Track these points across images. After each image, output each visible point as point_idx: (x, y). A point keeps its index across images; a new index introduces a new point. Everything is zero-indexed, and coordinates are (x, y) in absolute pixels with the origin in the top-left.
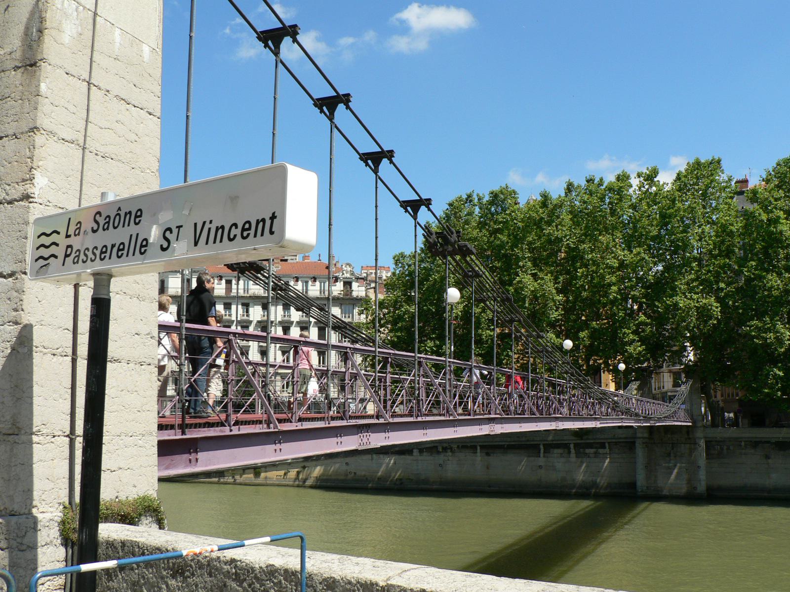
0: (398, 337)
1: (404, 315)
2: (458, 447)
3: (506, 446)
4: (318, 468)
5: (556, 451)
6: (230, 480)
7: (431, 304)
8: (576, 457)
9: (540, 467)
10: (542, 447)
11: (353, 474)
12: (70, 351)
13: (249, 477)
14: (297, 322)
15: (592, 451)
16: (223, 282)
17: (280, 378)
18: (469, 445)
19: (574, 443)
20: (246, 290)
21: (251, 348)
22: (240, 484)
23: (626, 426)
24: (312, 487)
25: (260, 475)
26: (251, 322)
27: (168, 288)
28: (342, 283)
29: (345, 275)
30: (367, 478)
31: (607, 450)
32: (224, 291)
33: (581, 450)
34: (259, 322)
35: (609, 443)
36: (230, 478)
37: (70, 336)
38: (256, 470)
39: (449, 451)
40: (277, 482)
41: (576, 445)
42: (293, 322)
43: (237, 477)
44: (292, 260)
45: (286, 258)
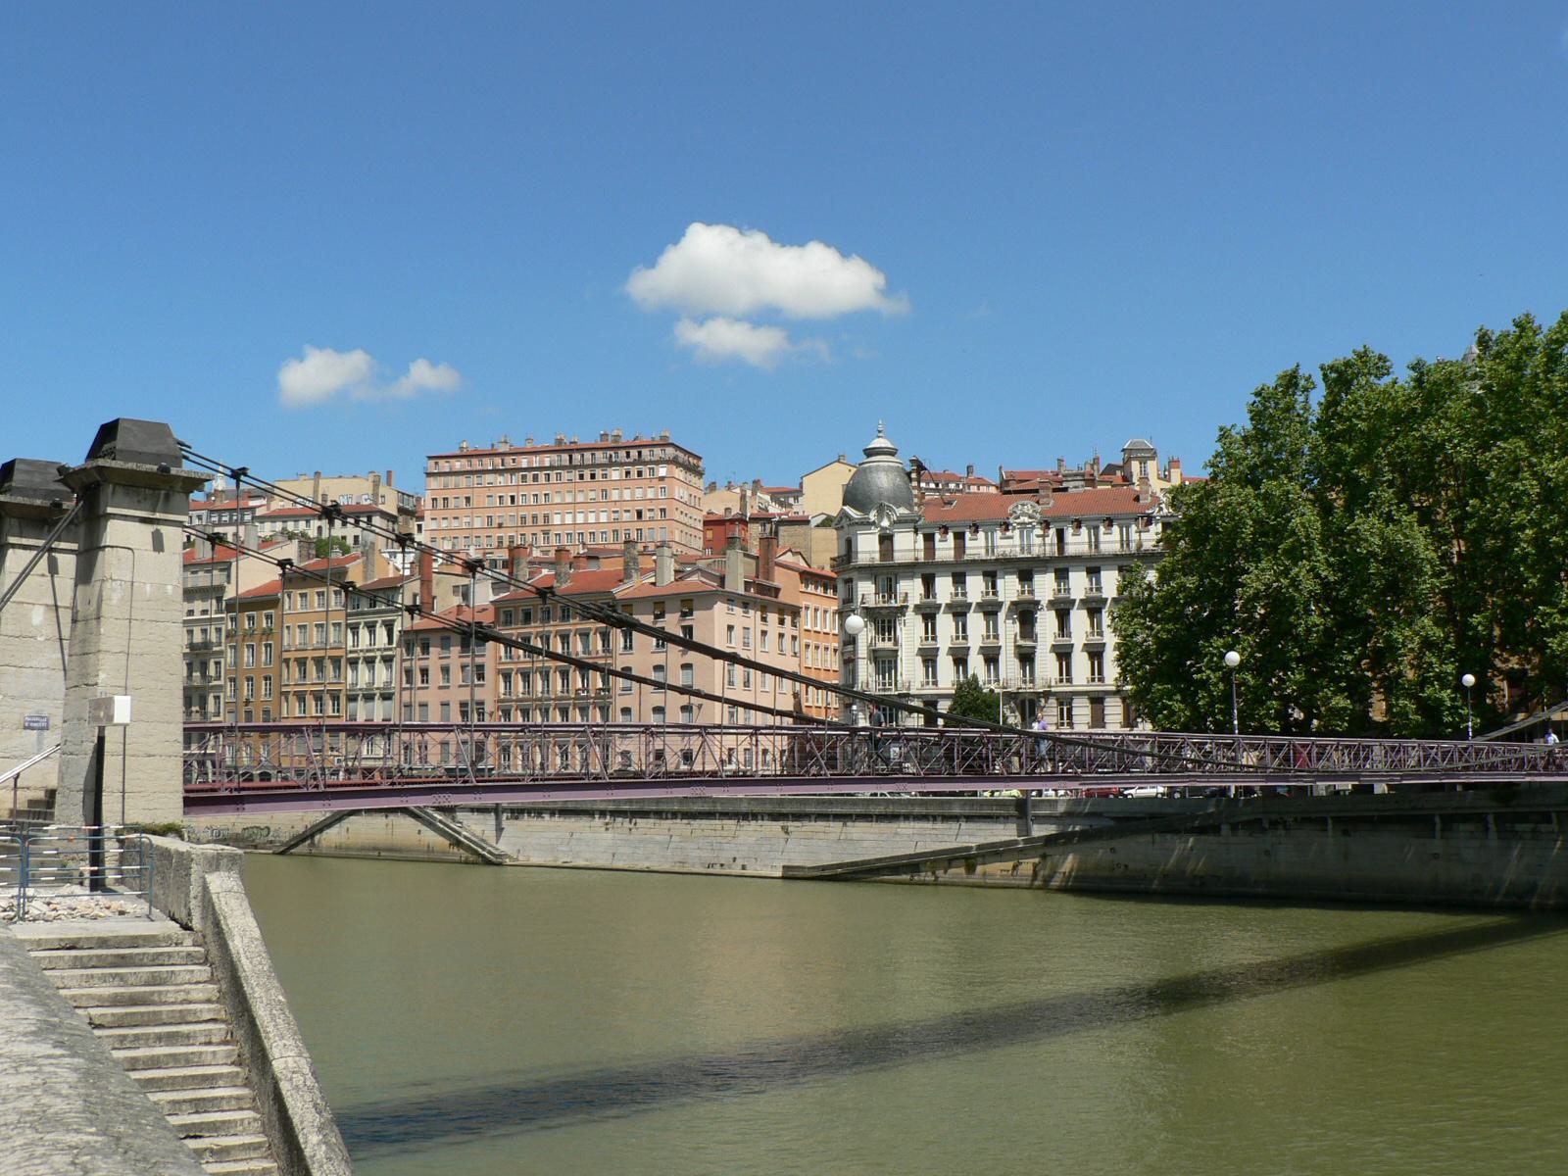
0: (1169, 631)
1: (1177, 594)
2: (1296, 820)
3: (1376, 818)
4: (1070, 857)
5: (1462, 827)
6: (930, 878)
7: (1218, 574)
8: (1499, 838)
9: (1436, 856)
10: (1437, 820)
11: (1123, 867)
12: (122, 753)
13: (958, 872)
14: (1082, 600)
15: (1527, 827)
16: (950, 536)
17: (1055, 701)
18: (1313, 816)
19: (1494, 813)
21: (1003, 651)
22: (945, 884)
24: (1063, 890)
25: (975, 870)
26: (1001, 604)
27: (857, 552)
28: (1160, 525)
29: (1165, 511)
31: (1555, 826)
32: (952, 552)
33: (1508, 825)
34: (1013, 603)
35: (1557, 812)
36: (929, 874)
37: (122, 746)
38: (968, 859)
39: (1280, 827)
41: (1499, 818)
43: (940, 873)
44: (1076, 487)
45: (1065, 485)
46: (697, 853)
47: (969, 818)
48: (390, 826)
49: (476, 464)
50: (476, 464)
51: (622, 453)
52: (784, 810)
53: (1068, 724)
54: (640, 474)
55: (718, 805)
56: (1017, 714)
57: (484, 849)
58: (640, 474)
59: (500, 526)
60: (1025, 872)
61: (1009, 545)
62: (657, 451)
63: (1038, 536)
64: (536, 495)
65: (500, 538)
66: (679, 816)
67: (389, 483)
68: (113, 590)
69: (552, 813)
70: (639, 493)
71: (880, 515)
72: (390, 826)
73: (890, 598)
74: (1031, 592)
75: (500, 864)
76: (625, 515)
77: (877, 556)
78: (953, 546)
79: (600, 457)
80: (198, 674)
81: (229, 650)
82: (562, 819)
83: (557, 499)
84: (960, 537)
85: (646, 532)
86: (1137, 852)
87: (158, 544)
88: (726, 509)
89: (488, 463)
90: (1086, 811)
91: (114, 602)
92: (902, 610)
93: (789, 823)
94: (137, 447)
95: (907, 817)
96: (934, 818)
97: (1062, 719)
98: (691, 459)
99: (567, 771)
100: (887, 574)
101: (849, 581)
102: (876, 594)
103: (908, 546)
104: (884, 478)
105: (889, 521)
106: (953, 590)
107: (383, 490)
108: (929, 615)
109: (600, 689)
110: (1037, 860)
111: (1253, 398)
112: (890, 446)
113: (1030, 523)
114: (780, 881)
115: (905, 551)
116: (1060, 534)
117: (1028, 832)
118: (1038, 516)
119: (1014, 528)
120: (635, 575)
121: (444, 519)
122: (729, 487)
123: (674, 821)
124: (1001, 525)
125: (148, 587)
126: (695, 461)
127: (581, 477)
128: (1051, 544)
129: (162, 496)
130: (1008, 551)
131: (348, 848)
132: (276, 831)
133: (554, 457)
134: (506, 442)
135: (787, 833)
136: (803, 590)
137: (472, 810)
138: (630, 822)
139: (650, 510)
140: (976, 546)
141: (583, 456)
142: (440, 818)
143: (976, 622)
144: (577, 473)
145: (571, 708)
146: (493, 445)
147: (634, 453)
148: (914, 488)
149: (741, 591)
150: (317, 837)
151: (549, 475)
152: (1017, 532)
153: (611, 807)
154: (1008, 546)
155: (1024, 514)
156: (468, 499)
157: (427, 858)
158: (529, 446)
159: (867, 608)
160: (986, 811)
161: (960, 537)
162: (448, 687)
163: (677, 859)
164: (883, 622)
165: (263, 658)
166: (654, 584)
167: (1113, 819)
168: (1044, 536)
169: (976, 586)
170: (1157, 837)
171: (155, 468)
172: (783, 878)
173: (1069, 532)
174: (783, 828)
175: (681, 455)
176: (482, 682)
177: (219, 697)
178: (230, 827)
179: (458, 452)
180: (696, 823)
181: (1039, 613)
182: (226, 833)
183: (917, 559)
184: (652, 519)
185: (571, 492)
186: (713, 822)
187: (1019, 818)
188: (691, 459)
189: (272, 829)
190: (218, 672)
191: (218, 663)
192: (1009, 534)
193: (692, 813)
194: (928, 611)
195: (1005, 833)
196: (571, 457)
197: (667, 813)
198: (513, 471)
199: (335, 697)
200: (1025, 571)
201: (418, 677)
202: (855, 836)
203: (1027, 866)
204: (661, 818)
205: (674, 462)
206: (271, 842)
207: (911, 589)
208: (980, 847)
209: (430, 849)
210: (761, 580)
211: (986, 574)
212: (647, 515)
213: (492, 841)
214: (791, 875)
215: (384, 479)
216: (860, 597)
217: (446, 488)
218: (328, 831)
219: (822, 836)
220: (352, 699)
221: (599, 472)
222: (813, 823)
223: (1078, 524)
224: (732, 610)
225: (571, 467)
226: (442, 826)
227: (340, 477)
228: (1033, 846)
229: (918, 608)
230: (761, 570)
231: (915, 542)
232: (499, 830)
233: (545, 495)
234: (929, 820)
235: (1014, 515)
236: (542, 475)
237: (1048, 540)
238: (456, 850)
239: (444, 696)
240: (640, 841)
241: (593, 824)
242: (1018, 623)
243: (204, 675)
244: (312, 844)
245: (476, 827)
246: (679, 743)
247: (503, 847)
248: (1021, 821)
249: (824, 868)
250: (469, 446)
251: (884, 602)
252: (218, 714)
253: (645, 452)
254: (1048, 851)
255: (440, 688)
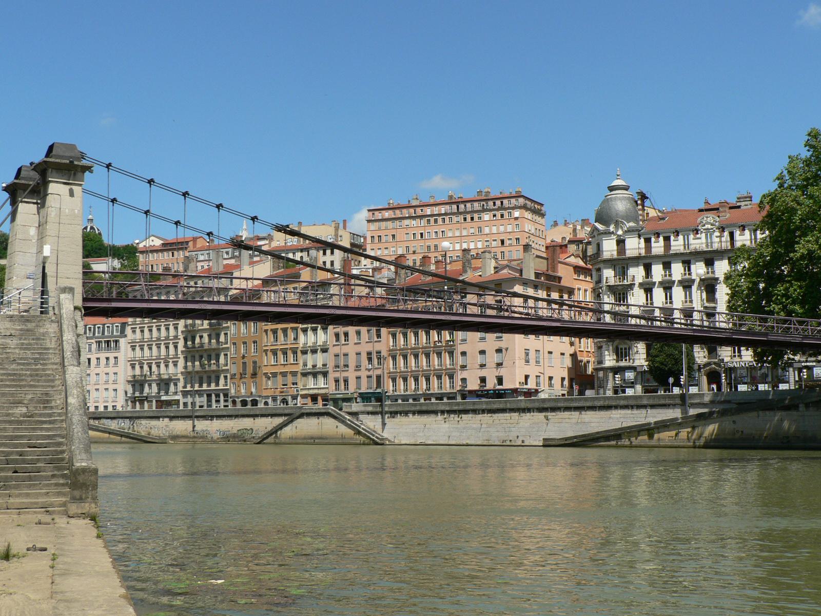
6: (627, 443)
11: (740, 433)
13: (644, 438)
14: (679, 281)
16: (661, 239)
20: (687, 245)
22: (636, 447)
23: (342, 315)
26: (693, 281)
30: (754, 437)
32: (663, 249)
36: (627, 440)
38: (649, 430)
40: (670, 444)
42: (674, 281)
43: (633, 439)
44: (746, 205)
46: (497, 434)
47: (653, 406)
48: (320, 424)
49: (398, 213)
50: (398, 213)
51: (491, 203)
52: (545, 406)
53: (739, 356)
54: (502, 216)
55: (508, 404)
56: (705, 350)
57: (373, 435)
58: (502, 216)
59: (414, 252)
60: (682, 437)
61: (698, 243)
62: (513, 201)
63: (717, 237)
64: (437, 232)
65: (414, 260)
66: (486, 411)
67: (345, 228)
68: (52, 211)
69: (414, 413)
70: (502, 229)
71: (617, 227)
72: (320, 424)
73: (624, 279)
74: (713, 272)
75: (382, 444)
76: (493, 243)
77: (615, 253)
78: (663, 245)
79: (477, 206)
80: (215, 341)
81: (232, 326)
82: (419, 417)
83: (450, 234)
84: (667, 239)
85: (506, 254)
86: (749, 422)
87: (72, 194)
88: (563, 238)
89: (406, 213)
90: (722, 400)
91: (53, 216)
92: (631, 286)
93: (549, 414)
94: (61, 154)
95: (616, 407)
96: (632, 407)
97: (734, 352)
98: (536, 206)
99: (430, 392)
100: (621, 264)
101: (599, 270)
102: (615, 277)
103: (634, 246)
104: (621, 205)
105: (622, 230)
106: (663, 273)
107: (341, 232)
108: (648, 289)
109: (448, 341)
110: (689, 430)
111: (807, 137)
112: (624, 184)
113: (712, 229)
114: (542, 448)
115: (632, 249)
116: (732, 235)
117: (687, 412)
118: (717, 224)
119: (702, 232)
120: (469, 270)
121: (379, 249)
122: (566, 224)
123: (483, 415)
124: (693, 231)
125: (67, 210)
126: (539, 207)
127: (465, 219)
128: (726, 242)
129: (72, 174)
130: (698, 246)
131: (296, 438)
132: (257, 430)
133: (448, 207)
134: (417, 199)
135: (547, 419)
136: (576, 278)
137: (368, 413)
138: (458, 417)
139: (509, 239)
140: (677, 245)
141: (465, 206)
142: (348, 418)
143: (678, 293)
144: (462, 217)
145: (431, 353)
146: (409, 201)
147: (498, 203)
148: (639, 210)
149: (533, 277)
150: (279, 432)
151: (444, 219)
152: (704, 235)
153: (448, 408)
154: (698, 244)
155: (708, 223)
156: (394, 236)
157: (343, 442)
158: (432, 201)
159: (609, 286)
160: (662, 402)
161: (667, 239)
162: (360, 343)
163: (485, 438)
164: (620, 294)
165: (252, 330)
166: (480, 276)
167: (737, 404)
168: (721, 237)
169: (677, 270)
170: (761, 413)
171: (68, 161)
172: (544, 446)
173: (737, 233)
174: (545, 416)
175: (529, 203)
176: (379, 340)
177: (227, 355)
178: (230, 429)
179: (387, 207)
180: (496, 416)
181: (718, 285)
182: (228, 433)
183: (640, 254)
184: (510, 245)
185: (458, 229)
186: (505, 415)
187: (681, 405)
188: (536, 206)
189: (254, 430)
190: (226, 339)
191: (226, 334)
192: (698, 236)
193: (493, 410)
194: (648, 286)
195: (675, 413)
196: (458, 207)
197: (479, 410)
198: (421, 217)
199: (295, 352)
200: (709, 259)
201: (342, 338)
202: (587, 420)
203: (684, 433)
204: (476, 414)
205: (524, 207)
206: (254, 437)
207: (637, 273)
208: (656, 423)
209: (343, 437)
210: (550, 273)
211: (684, 262)
212: (507, 242)
213: (380, 431)
214: (548, 444)
215: (341, 225)
216: (605, 279)
217: (379, 229)
218: (285, 429)
219: (567, 420)
220: (304, 352)
221: (476, 216)
222: (562, 413)
223: (743, 228)
224: (527, 290)
225: (458, 213)
226: (349, 423)
227: (314, 225)
228: (686, 421)
229: (641, 285)
230: (550, 266)
231: (639, 243)
232: (384, 424)
233: (442, 232)
234: (629, 409)
235: (702, 224)
236: (440, 219)
237: (724, 239)
238: (357, 437)
239: (358, 348)
240: (464, 428)
241: (437, 419)
242: (705, 293)
243: (218, 342)
244: (276, 437)
245: (371, 423)
246: (495, 372)
247: (385, 435)
248: (683, 407)
249: (566, 439)
250: (394, 202)
251: (620, 282)
252: (227, 365)
253: (505, 202)
254: (696, 424)
255: (355, 344)
